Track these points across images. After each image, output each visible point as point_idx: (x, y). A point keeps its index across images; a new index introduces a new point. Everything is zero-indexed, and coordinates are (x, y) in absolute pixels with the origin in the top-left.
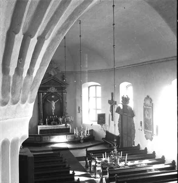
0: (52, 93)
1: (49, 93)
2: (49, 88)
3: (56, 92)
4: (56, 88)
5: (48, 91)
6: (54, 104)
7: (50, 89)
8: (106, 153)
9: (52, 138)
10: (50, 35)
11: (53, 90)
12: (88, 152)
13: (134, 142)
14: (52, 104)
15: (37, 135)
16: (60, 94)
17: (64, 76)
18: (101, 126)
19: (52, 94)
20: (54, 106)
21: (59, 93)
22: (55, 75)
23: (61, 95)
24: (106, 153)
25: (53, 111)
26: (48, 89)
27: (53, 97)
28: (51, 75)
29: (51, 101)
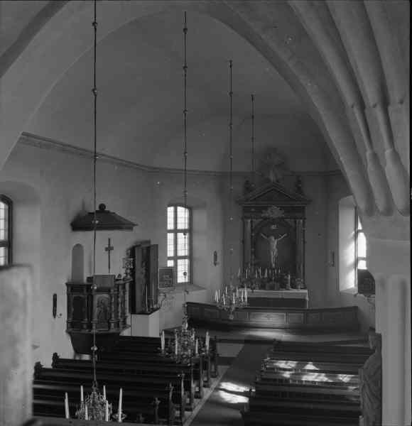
0: (273, 220)
1: (265, 219)
3: (283, 218)
5: (263, 215)
6: (274, 243)
8: (84, 388)
9: (254, 315)
13: (380, 336)
14: (272, 244)
16: (290, 222)
17: (299, 182)
18: (366, 298)
19: (273, 222)
20: (275, 247)
22: (278, 181)
23: (293, 225)
24: (82, 387)
25: (273, 260)
26: (264, 211)
27: (273, 227)
28: (268, 180)
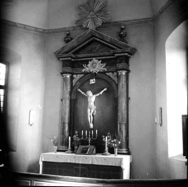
1: (86, 73)
2: (87, 63)
3: (104, 73)
4: (103, 61)
5: (83, 70)
6: (92, 98)
7: (89, 65)
10: (123, 128)
11: (96, 66)
12: (114, 55)
15: (38, 174)
16: (75, 142)
21: (110, 74)
26: (84, 66)
29: (85, 92)
